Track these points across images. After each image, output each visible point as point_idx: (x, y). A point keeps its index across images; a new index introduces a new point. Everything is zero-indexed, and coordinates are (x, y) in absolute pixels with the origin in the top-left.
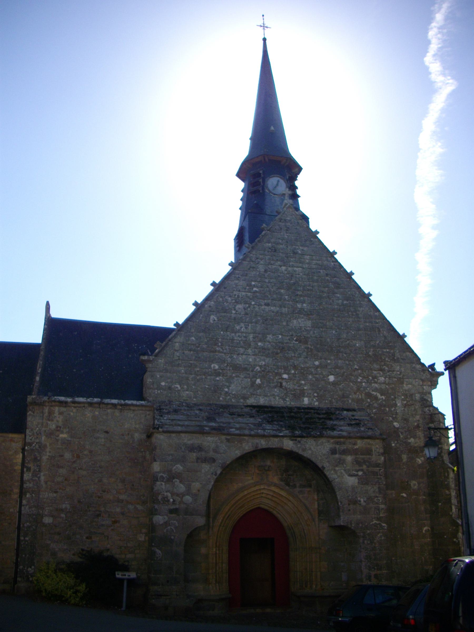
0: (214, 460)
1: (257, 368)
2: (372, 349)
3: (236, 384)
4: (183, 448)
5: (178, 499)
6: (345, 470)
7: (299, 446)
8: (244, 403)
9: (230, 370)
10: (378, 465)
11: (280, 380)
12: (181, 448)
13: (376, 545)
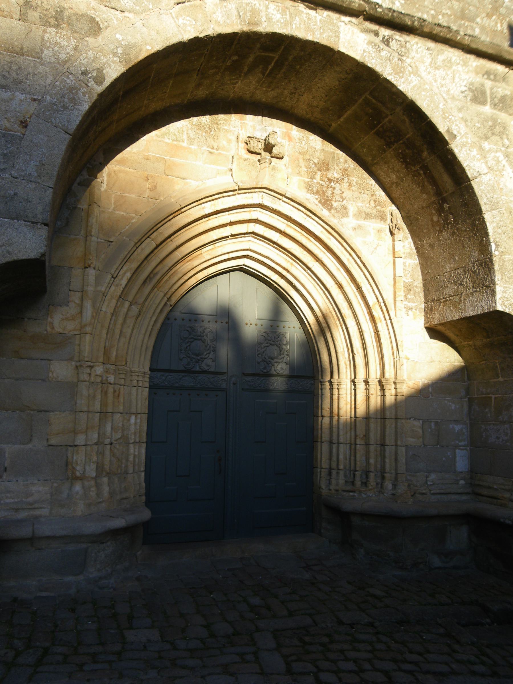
7: (383, 53)
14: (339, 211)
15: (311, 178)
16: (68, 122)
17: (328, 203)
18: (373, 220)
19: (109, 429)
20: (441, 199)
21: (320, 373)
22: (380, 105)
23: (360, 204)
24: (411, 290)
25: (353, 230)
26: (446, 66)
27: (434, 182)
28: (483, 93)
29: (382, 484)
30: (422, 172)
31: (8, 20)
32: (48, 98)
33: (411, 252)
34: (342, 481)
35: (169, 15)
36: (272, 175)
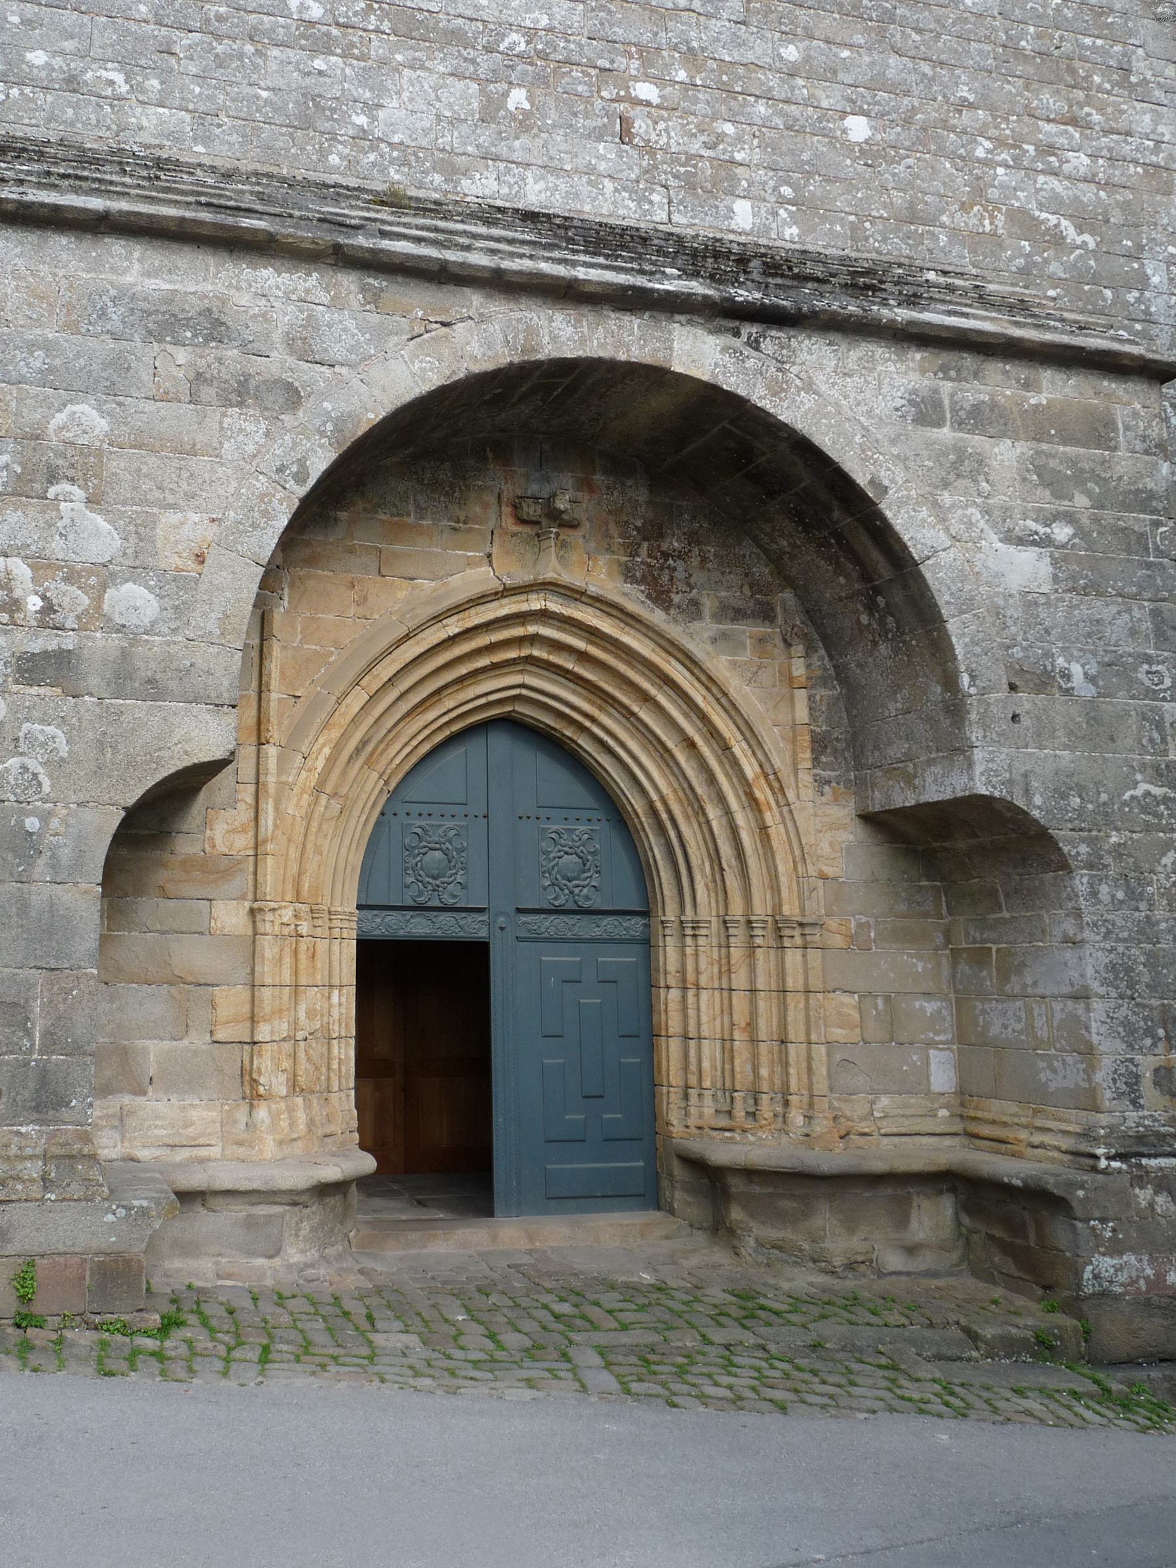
0: (293, 397)
1: (514, 37)
2: (1032, 29)
3: (411, 100)
4: (115, 315)
5: (74, 599)
6: (986, 511)
7: (750, 363)
8: (446, 192)
9: (383, 33)
10: (1142, 501)
11: (621, 107)
12: (103, 314)
13: (1159, 914)
18: (750, 621)
19: (302, 1015)
20: (872, 588)
21: (660, 905)
23: (724, 594)
24: (826, 747)
26: (864, 368)
27: (857, 560)
28: (937, 405)
29: (784, 1116)
30: (833, 541)
31: (174, 405)
32: (232, 514)
34: (709, 1111)
36: (562, 557)
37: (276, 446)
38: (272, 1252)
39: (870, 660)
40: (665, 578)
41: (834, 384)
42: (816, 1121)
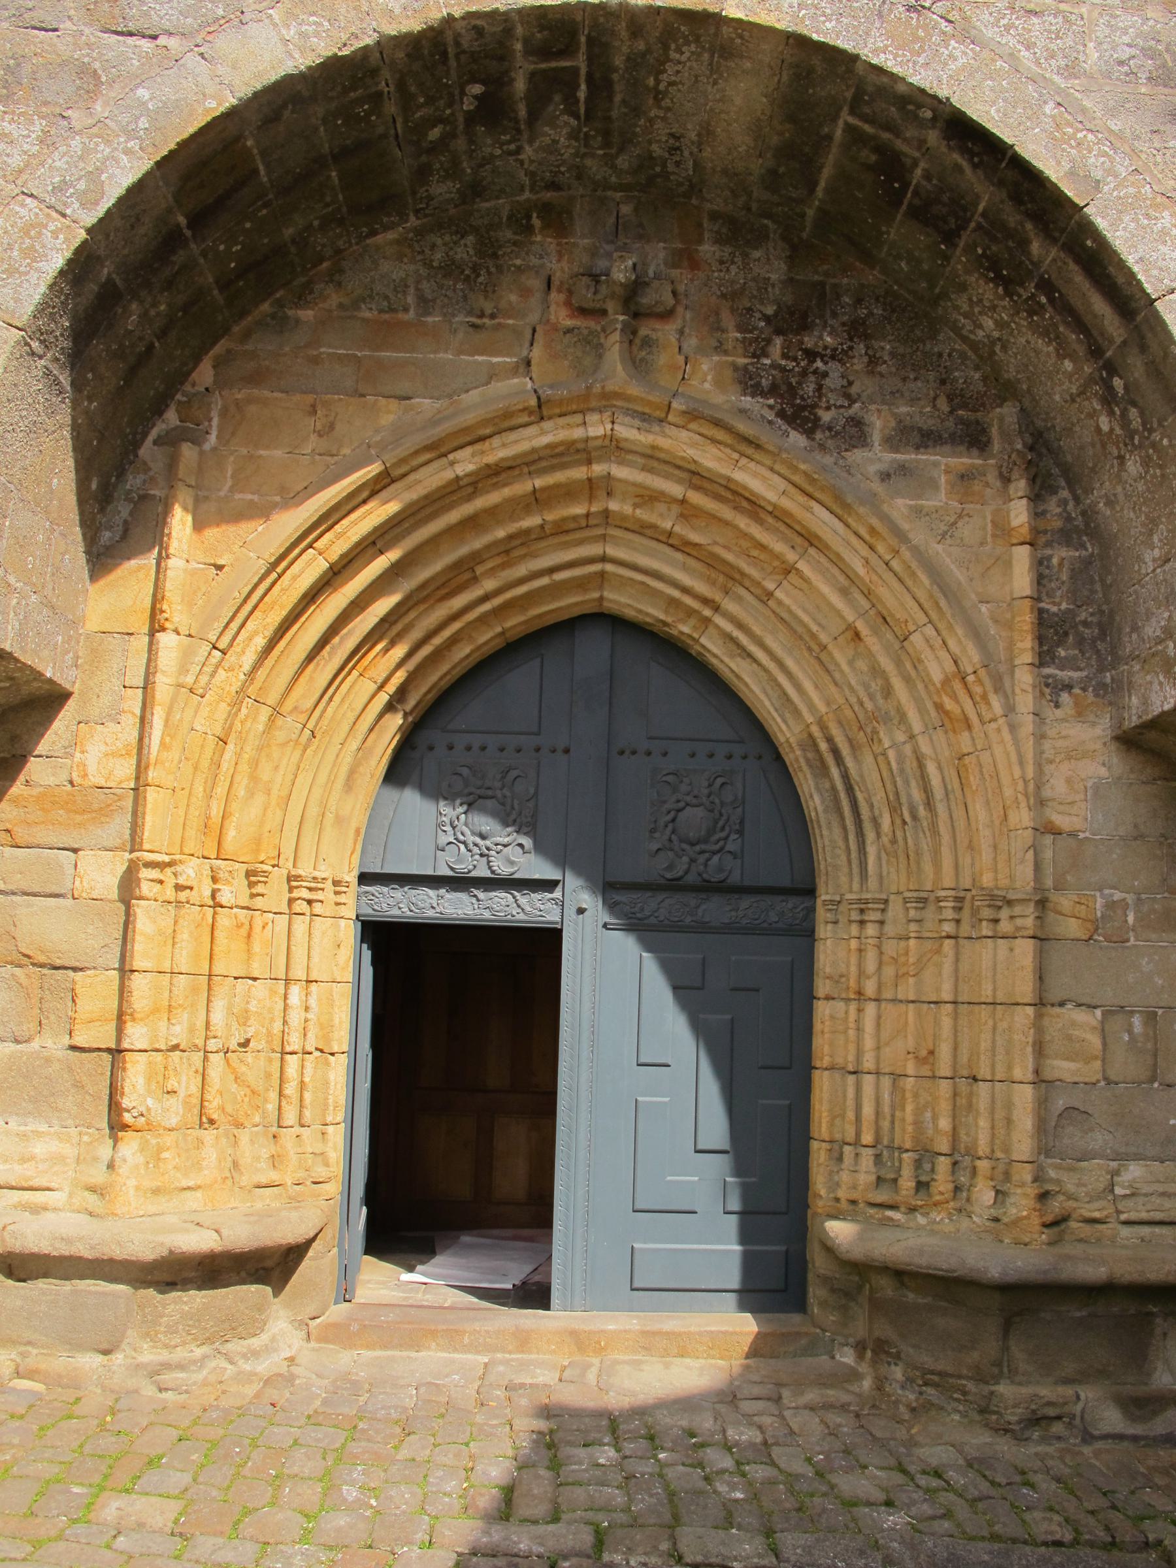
14: (837, 433)
15: (754, 356)
16: (15, 302)
17: (807, 414)
18: (947, 448)
22: (886, 135)
23: (904, 409)
24: (1066, 634)
25: (883, 480)
30: (1043, 300)
33: (1069, 526)
35: (267, 21)
37: (56, 155)
38: (105, 1346)
39: (1119, 489)
40: (809, 388)
41: (1007, 28)
42: (1012, 1200)
